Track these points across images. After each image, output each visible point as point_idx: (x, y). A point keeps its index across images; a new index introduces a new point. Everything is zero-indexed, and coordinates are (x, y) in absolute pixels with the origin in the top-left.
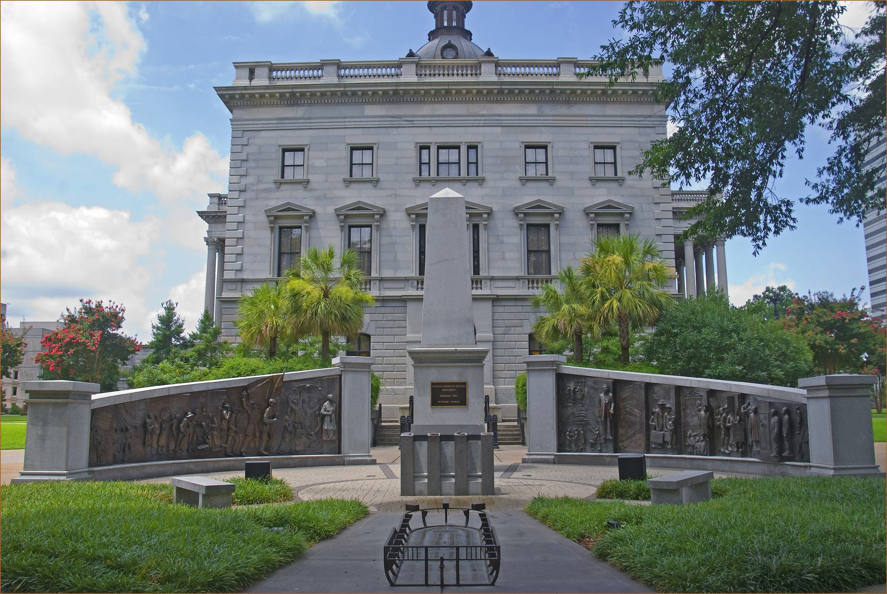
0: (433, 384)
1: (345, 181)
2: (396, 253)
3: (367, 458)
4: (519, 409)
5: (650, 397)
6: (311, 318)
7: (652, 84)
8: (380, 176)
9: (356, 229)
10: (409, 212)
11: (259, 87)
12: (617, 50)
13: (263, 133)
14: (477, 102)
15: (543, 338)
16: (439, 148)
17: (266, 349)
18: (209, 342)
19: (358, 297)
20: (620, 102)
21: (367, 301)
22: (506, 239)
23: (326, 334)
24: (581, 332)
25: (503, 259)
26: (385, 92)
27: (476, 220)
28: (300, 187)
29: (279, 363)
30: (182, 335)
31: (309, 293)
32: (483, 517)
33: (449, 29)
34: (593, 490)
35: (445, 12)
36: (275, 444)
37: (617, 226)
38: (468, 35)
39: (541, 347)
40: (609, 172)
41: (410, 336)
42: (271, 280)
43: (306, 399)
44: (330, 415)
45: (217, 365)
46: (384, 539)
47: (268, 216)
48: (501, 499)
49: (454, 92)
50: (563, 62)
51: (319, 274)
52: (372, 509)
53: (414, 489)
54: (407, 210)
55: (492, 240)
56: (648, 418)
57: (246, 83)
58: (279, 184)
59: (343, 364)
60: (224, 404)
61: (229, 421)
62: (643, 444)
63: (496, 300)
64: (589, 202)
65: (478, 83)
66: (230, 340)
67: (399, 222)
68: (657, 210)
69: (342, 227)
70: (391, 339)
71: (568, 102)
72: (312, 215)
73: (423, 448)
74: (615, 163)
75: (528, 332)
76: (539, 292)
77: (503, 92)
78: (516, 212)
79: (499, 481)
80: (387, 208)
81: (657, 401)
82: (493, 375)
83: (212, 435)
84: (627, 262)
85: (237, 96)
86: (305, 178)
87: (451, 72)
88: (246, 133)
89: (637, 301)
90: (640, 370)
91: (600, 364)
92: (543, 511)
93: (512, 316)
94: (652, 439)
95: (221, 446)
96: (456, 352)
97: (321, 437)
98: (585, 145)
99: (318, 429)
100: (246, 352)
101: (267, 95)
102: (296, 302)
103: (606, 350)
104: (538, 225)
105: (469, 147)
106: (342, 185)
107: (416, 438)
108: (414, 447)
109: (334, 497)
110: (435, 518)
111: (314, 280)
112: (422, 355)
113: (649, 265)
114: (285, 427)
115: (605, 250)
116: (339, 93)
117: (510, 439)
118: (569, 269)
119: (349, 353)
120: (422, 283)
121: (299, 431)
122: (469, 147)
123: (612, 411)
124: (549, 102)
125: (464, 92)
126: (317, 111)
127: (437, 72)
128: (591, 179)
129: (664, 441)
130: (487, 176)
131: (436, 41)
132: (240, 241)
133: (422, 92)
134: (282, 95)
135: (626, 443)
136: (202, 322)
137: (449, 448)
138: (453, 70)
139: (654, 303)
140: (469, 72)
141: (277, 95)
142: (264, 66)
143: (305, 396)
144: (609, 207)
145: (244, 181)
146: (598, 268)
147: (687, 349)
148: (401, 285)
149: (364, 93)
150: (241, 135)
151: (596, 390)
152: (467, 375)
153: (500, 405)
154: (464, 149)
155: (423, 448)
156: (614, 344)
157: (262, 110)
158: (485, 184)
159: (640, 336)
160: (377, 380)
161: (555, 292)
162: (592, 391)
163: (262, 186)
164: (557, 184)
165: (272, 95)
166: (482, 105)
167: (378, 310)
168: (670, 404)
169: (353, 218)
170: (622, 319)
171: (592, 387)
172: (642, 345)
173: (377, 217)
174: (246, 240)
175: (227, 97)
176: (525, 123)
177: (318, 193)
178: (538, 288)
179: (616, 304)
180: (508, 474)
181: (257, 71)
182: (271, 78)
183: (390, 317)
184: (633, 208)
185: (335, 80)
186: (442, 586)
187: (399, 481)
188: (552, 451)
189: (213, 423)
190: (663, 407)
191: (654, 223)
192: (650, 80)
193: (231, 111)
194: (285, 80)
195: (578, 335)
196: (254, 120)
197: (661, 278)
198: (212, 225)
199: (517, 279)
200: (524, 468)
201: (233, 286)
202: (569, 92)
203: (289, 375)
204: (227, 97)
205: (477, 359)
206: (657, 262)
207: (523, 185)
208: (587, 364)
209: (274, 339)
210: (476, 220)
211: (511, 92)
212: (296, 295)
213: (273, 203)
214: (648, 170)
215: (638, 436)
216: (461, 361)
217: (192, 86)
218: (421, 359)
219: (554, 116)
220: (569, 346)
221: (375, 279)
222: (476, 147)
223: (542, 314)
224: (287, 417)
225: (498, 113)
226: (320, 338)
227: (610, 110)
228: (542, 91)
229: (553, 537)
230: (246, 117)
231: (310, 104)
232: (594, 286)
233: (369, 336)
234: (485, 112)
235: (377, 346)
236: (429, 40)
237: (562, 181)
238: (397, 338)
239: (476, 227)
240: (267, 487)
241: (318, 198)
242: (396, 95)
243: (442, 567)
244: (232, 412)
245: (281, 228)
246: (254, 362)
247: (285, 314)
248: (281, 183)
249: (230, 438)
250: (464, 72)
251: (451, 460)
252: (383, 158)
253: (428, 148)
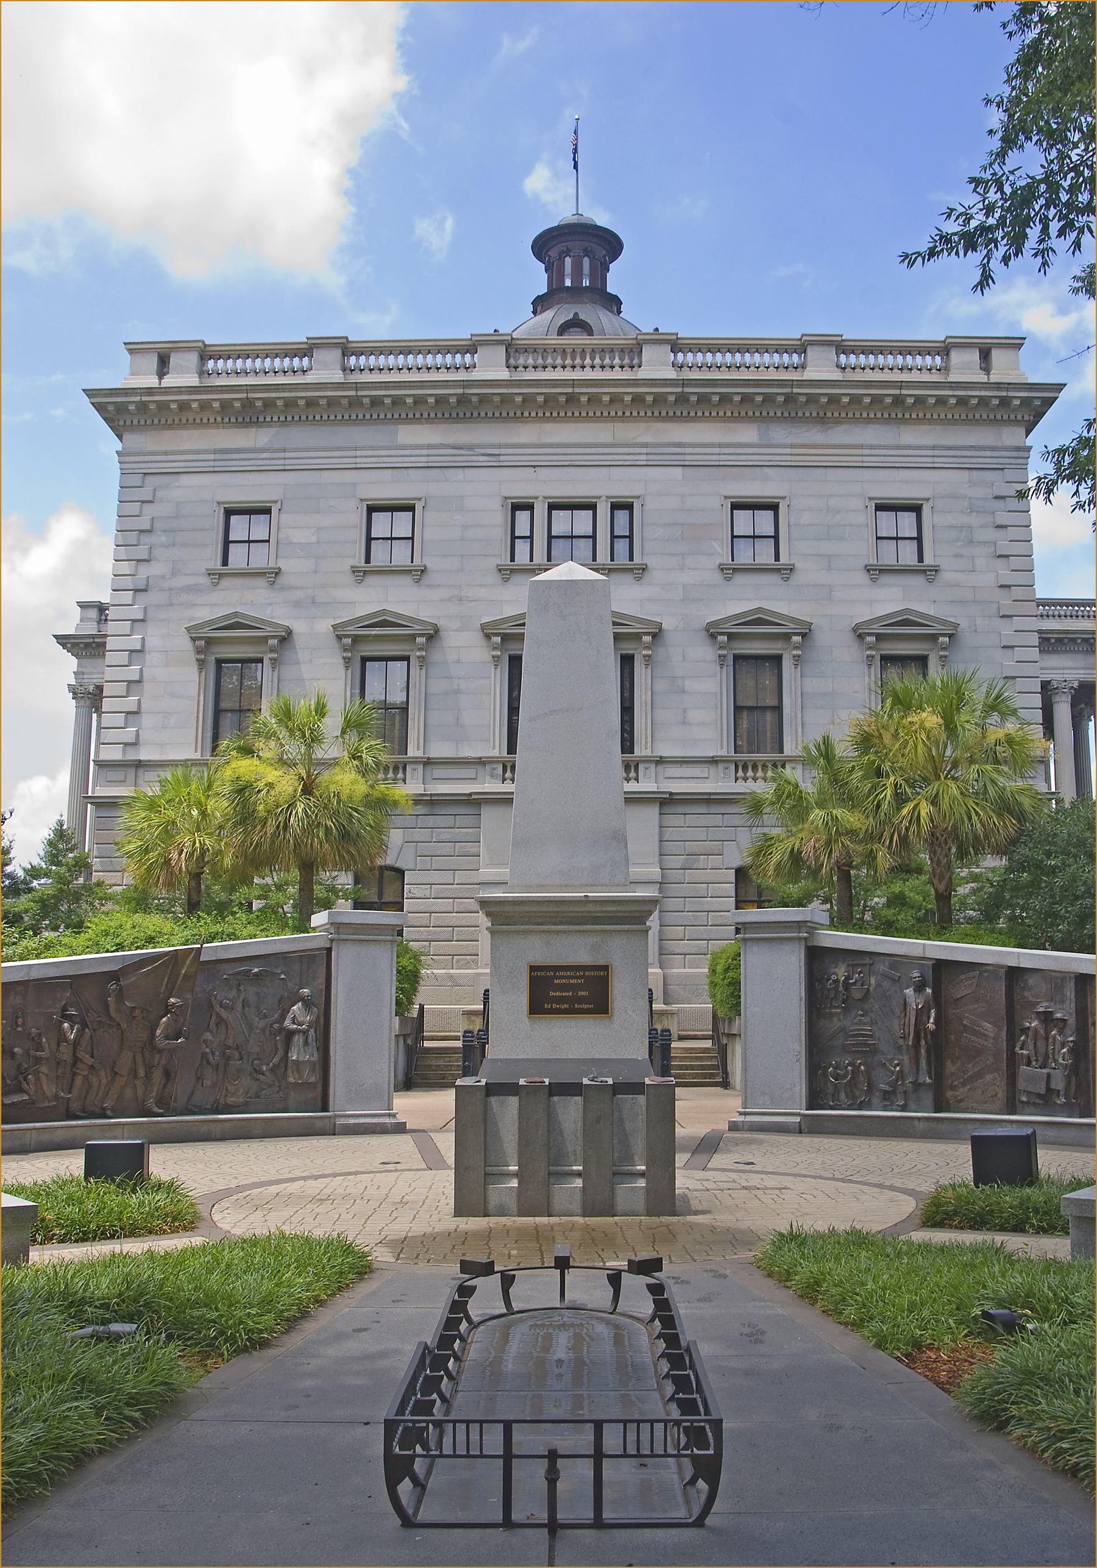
0: (533, 968)
1: (355, 570)
2: (461, 708)
3: (387, 1120)
4: (715, 1016)
5: (1016, 997)
6: (275, 835)
7: (998, 386)
8: (429, 562)
9: (377, 664)
10: (487, 632)
11: (179, 390)
12: (1008, 190)
13: (185, 480)
14: (631, 418)
15: (768, 878)
16: (552, 507)
17: (181, 895)
18: (60, 879)
19: (376, 794)
20: (931, 421)
21: (395, 803)
22: (689, 685)
23: (308, 868)
24: (850, 865)
25: (684, 722)
26: (440, 400)
27: (628, 648)
28: (261, 582)
29: (206, 923)
30: (8, 869)
31: (271, 786)
32: (656, 1290)
33: (577, 293)
34: (908, 1206)
35: (568, 261)
36: (180, 1090)
37: (922, 661)
38: (614, 303)
39: (760, 894)
40: (908, 554)
41: (487, 872)
42: (194, 763)
43: (252, 998)
44: (305, 1032)
45: (78, 927)
46: (403, 1364)
47: (194, 639)
48: (691, 1226)
49: (584, 399)
50: (813, 343)
51: (294, 749)
52: (382, 1256)
53: (485, 1202)
54: (483, 627)
55: (661, 685)
56: (1011, 1040)
57: (152, 381)
58: (216, 577)
59: (337, 926)
60: (65, 1009)
61: (76, 1043)
62: (1001, 1094)
63: (667, 802)
64: (863, 614)
65: (635, 382)
66: (109, 878)
67: (466, 652)
68: (1007, 629)
69: (347, 661)
70: (447, 877)
71: (822, 420)
72: (286, 638)
73: (507, 1112)
74: (919, 539)
75: (738, 863)
76: (762, 788)
77: (687, 400)
78: (712, 632)
79: (685, 1181)
80: (441, 623)
81: (1035, 1004)
82: (660, 948)
83: (37, 1073)
84: (950, 727)
85: (132, 407)
86: (272, 564)
87: (578, 361)
88: (148, 478)
89: (971, 803)
90: (976, 939)
91: (888, 928)
92: (807, 1269)
93: (701, 834)
94: (1021, 1084)
95: (56, 1097)
96: (586, 901)
97: (285, 1075)
98: (857, 503)
99: (276, 1060)
100: (140, 901)
101: (195, 405)
102: (244, 803)
103: (897, 901)
104: (757, 660)
105: (615, 507)
106: (350, 579)
107: (491, 1090)
108: (486, 1108)
109: (287, 1229)
110: (536, 1289)
111: (283, 762)
112: (509, 908)
113: (996, 733)
114: (204, 1056)
115: (903, 703)
116: (345, 402)
117: (696, 1076)
118: (826, 741)
119: (358, 905)
120: (513, 768)
121: (235, 1063)
122: (615, 507)
123: (931, 1026)
124: (783, 419)
125: (606, 398)
126: (298, 436)
127: (549, 361)
128: (868, 569)
129: (1049, 1090)
130: (650, 561)
131: (548, 315)
132: (133, 686)
133: (519, 399)
134: (225, 405)
135: (962, 1092)
136: (51, 843)
137: (570, 1113)
138: (583, 358)
139: (1006, 806)
140: (617, 361)
141: (216, 405)
142: (189, 349)
143: (250, 992)
144: (906, 623)
145: (144, 571)
146: (887, 739)
147: (1077, 898)
148: (470, 772)
149: (397, 401)
150: (137, 482)
151: (895, 981)
152: (614, 951)
153: (674, 1007)
154: (604, 510)
155: (507, 1112)
156: (916, 888)
157: (184, 433)
158: (647, 577)
159: (971, 874)
160: (416, 957)
161: (797, 786)
162: (885, 984)
163: (181, 581)
164: (798, 578)
165: (205, 406)
166: (643, 425)
167: (421, 821)
168: (1064, 1011)
169: (371, 645)
170: (935, 840)
171: (885, 976)
172: (974, 892)
173: (421, 640)
174: (146, 686)
175: (111, 408)
176: (732, 460)
177: (299, 594)
178: (755, 779)
179: (925, 809)
180: (701, 1158)
181: (174, 360)
182: (202, 373)
183: (446, 835)
184: (956, 626)
185: (338, 377)
186: (553, 1527)
187: (451, 1174)
188: (797, 1108)
189: (39, 1047)
190: (1047, 1018)
191: (999, 655)
192: (994, 378)
193: (120, 437)
194: (227, 375)
195: (844, 871)
196: (166, 453)
197: (1015, 756)
198: (84, 661)
199: (713, 761)
200: (736, 1143)
201: (119, 775)
202: (824, 400)
203: (214, 949)
204: (111, 408)
205: (630, 917)
206: (1011, 727)
207: (728, 579)
208: (860, 927)
209: (197, 876)
210: (628, 648)
211: (703, 399)
212: (243, 790)
213: (204, 614)
214: (1065, 489)
215: (989, 1077)
216: (596, 920)
217: (59, 412)
218: (505, 917)
219: (792, 446)
220: (821, 893)
221: (416, 761)
222: (629, 507)
223: (766, 830)
224: (208, 1036)
225: (677, 439)
226: (295, 874)
227: (910, 435)
228: (768, 399)
229: (841, 1346)
230: (151, 447)
231: (285, 423)
232: (879, 773)
233: (401, 873)
234: (648, 439)
235: (417, 891)
236: (535, 312)
237: (808, 572)
238: (460, 877)
239: (627, 662)
240: (134, 1200)
241: (297, 604)
242: (465, 405)
243: (552, 1477)
244: (84, 1025)
245: (219, 662)
246: (153, 922)
247: (221, 827)
248: (221, 575)
249: (79, 1081)
250: (607, 361)
251: (571, 1138)
252: (434, 527)
253: (530, 507)
